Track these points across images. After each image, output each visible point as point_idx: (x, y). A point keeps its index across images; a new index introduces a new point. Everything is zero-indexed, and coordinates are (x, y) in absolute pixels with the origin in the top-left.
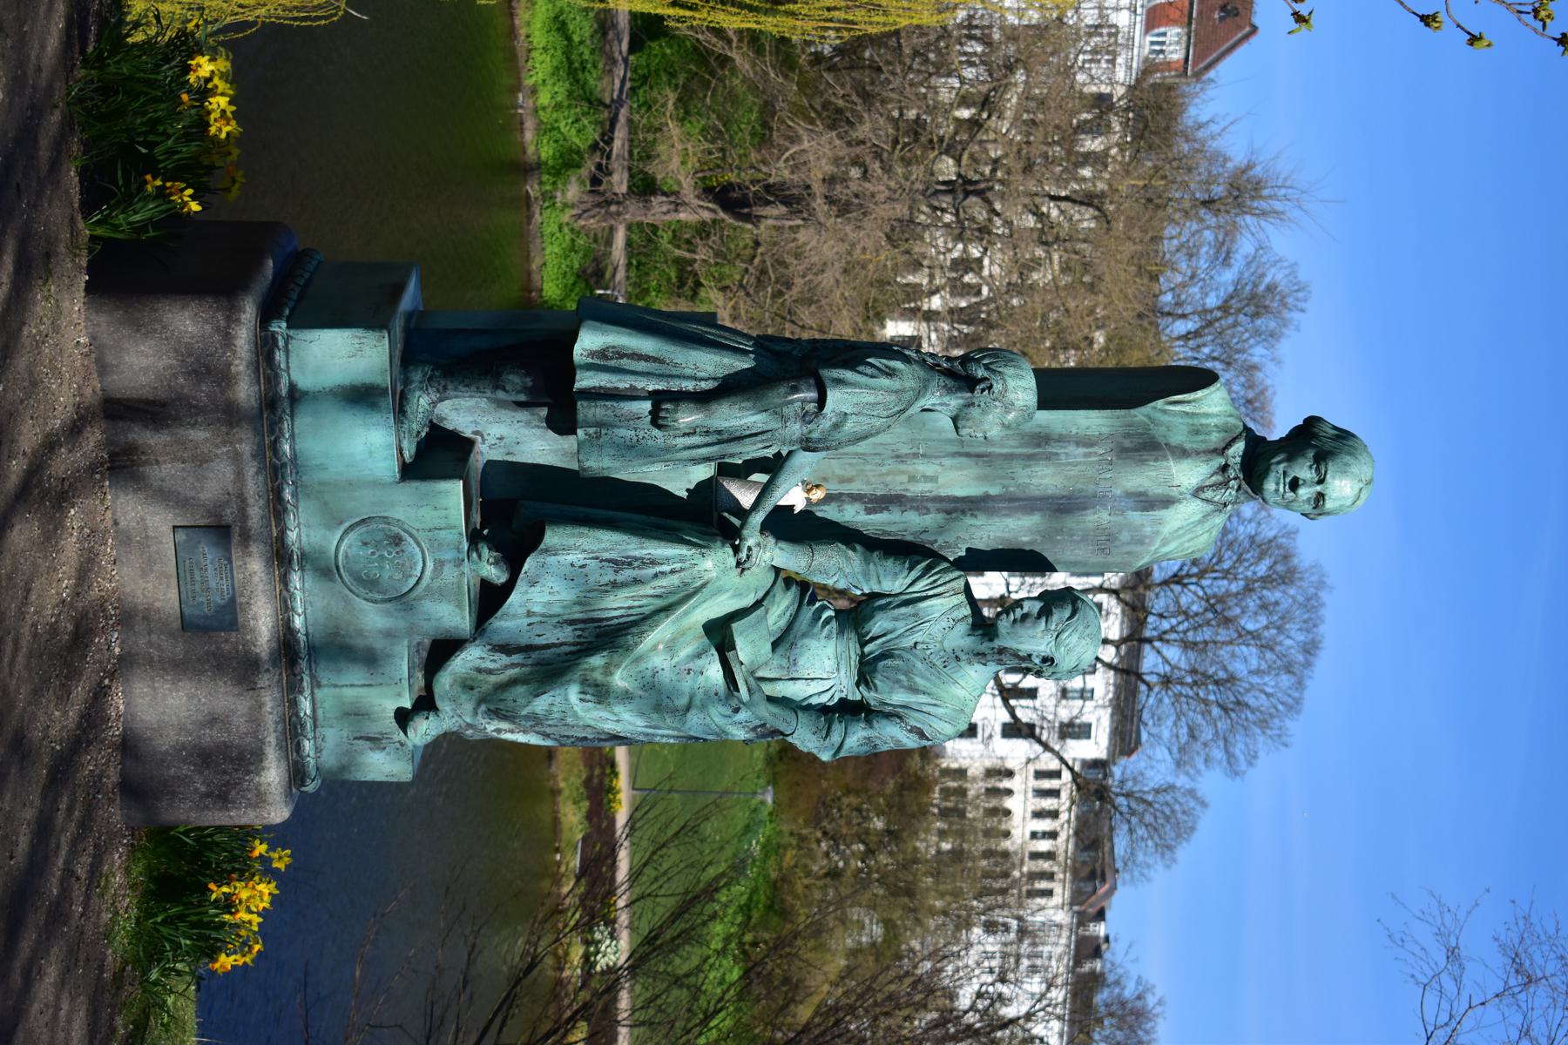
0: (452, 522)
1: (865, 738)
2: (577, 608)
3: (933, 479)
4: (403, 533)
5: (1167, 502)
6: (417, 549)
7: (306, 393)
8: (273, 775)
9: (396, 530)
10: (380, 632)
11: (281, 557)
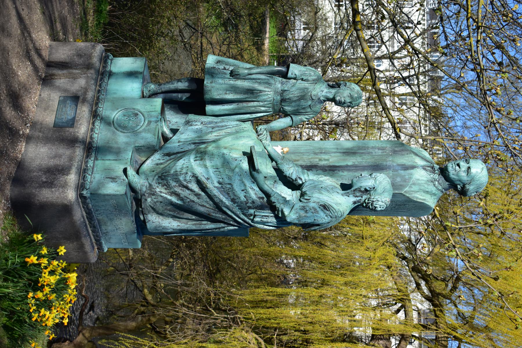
0: (156, 110)
1: (302, 206)
2: (197, 139)
3: (328, 160)
4: (139, 113)
5: (413, 167)
6: (143, 118)
7: (115, 73)
8: (72, 178)
9: (136, 112)
10: (124, 143)
11: (95, 115)
